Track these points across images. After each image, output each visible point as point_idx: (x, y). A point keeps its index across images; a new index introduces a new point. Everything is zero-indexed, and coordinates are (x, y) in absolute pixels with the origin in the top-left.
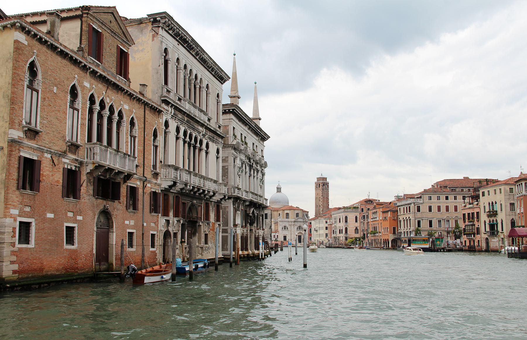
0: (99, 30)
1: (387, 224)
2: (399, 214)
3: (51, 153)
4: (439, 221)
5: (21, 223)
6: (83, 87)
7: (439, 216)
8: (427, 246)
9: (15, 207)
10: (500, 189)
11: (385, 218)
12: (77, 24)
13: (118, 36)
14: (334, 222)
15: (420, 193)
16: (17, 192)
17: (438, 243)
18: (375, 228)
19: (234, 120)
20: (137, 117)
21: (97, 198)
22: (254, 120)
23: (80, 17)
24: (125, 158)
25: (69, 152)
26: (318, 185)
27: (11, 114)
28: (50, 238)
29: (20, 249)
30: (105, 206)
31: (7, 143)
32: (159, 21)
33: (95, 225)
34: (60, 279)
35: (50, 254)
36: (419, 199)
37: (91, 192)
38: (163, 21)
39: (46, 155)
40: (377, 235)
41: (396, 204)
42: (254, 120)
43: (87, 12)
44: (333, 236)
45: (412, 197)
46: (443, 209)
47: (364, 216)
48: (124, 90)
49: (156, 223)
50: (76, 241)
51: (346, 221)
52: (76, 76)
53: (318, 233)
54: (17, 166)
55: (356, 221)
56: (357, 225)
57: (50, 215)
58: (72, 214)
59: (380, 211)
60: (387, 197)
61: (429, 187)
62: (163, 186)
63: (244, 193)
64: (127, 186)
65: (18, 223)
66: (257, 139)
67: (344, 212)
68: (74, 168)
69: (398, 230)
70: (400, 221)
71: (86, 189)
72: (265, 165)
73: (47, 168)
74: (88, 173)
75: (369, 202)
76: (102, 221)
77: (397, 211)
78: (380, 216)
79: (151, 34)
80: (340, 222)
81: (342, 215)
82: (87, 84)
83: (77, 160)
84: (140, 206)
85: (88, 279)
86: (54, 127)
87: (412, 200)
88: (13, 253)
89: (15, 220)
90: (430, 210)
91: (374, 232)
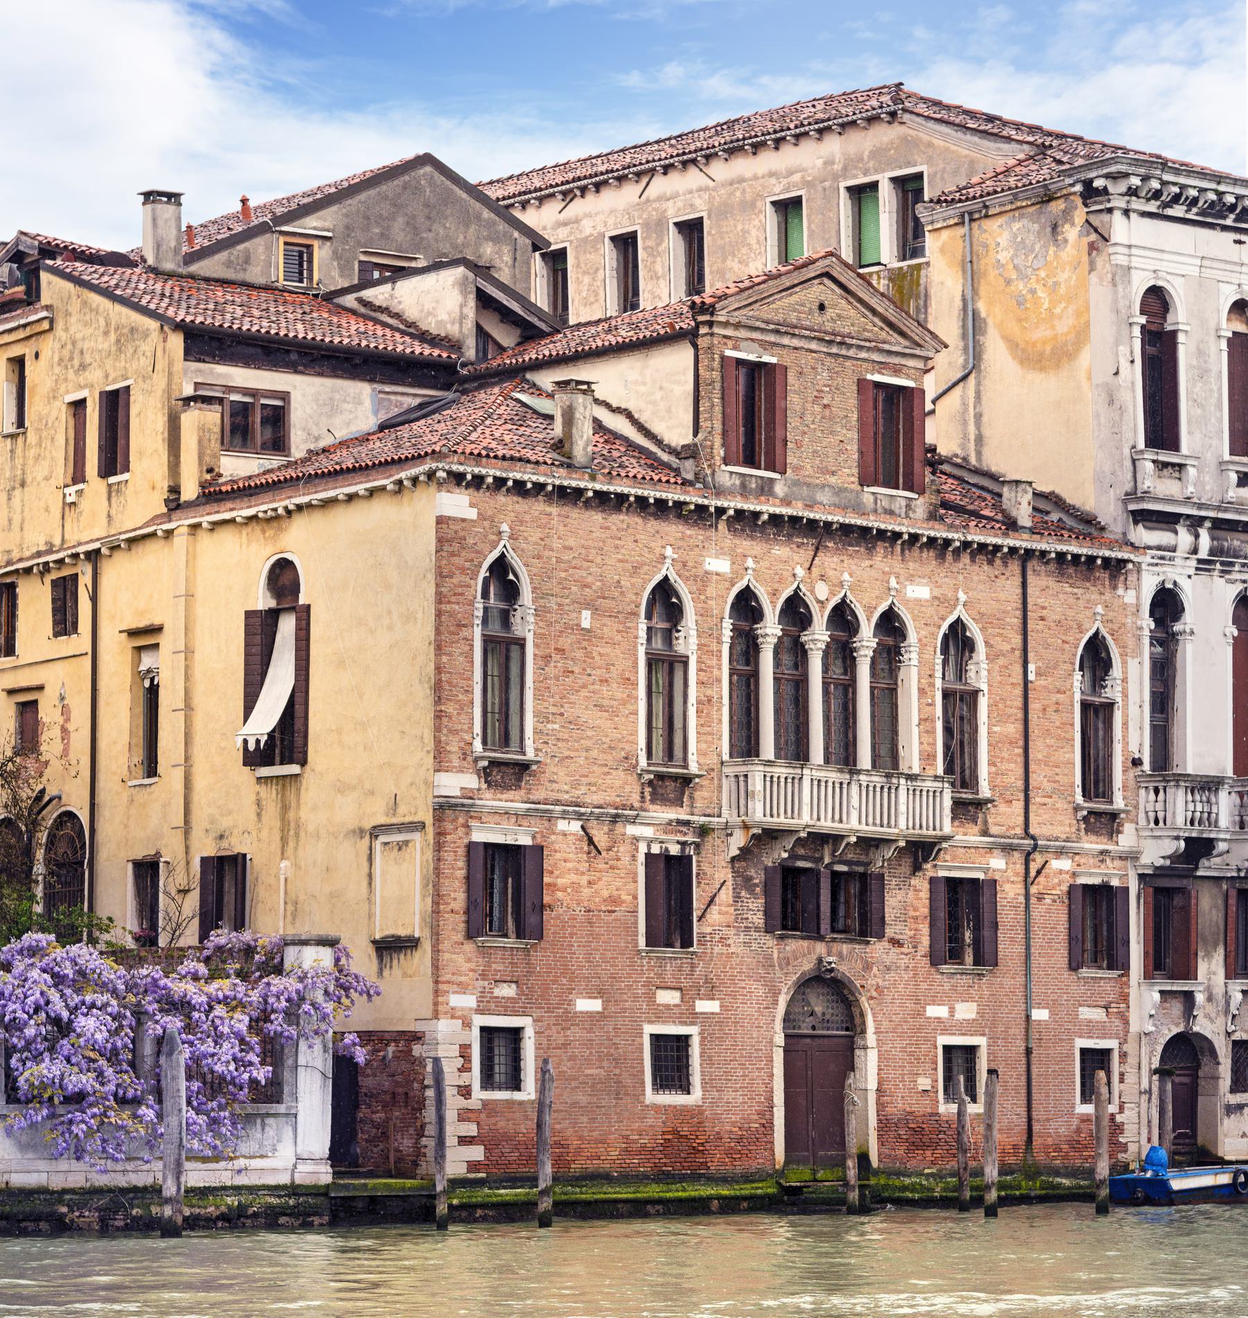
3: (579, 816)
5: (484, 1030)
6: (702, 580)
9: (463, 988)
10: (934, 829)
12: (679, 359)
13: (860, 348)
16: (469, 947)
20: (980, 618)
21: (782, 938)
23: (690, 336)
25: (653, 801)
27: (438, 729)
28: (588, 1072)
29: (485, 1103)
30: (820, 960)
31: (431, 811)
32: (1105, 191)
33: (778, 1025)
35: (593, 1120)
37: (758, 919)
38: (1122, 187)
39: (562, 825)
43: (707, 318)
48: (897, 535)
49: (1118, 1006)
50: (696, 1079)
52: (669, 551)
54: (461, 873)
57: (588, 1005)
58: (677, 994)
62: (1146, 859)
64: (932, 881)
65: (476, 1033)
68: (674, 850)
71: (726, 909)
73: (569, 865)
74: (733, 859)
76: (818, 1009)
79: (1086, 240)
82: (719, 565)
83: (687, 823)
84: (1008, 947)
86: (589, 733)
88: (465, 1115)
89: (467, 1024)
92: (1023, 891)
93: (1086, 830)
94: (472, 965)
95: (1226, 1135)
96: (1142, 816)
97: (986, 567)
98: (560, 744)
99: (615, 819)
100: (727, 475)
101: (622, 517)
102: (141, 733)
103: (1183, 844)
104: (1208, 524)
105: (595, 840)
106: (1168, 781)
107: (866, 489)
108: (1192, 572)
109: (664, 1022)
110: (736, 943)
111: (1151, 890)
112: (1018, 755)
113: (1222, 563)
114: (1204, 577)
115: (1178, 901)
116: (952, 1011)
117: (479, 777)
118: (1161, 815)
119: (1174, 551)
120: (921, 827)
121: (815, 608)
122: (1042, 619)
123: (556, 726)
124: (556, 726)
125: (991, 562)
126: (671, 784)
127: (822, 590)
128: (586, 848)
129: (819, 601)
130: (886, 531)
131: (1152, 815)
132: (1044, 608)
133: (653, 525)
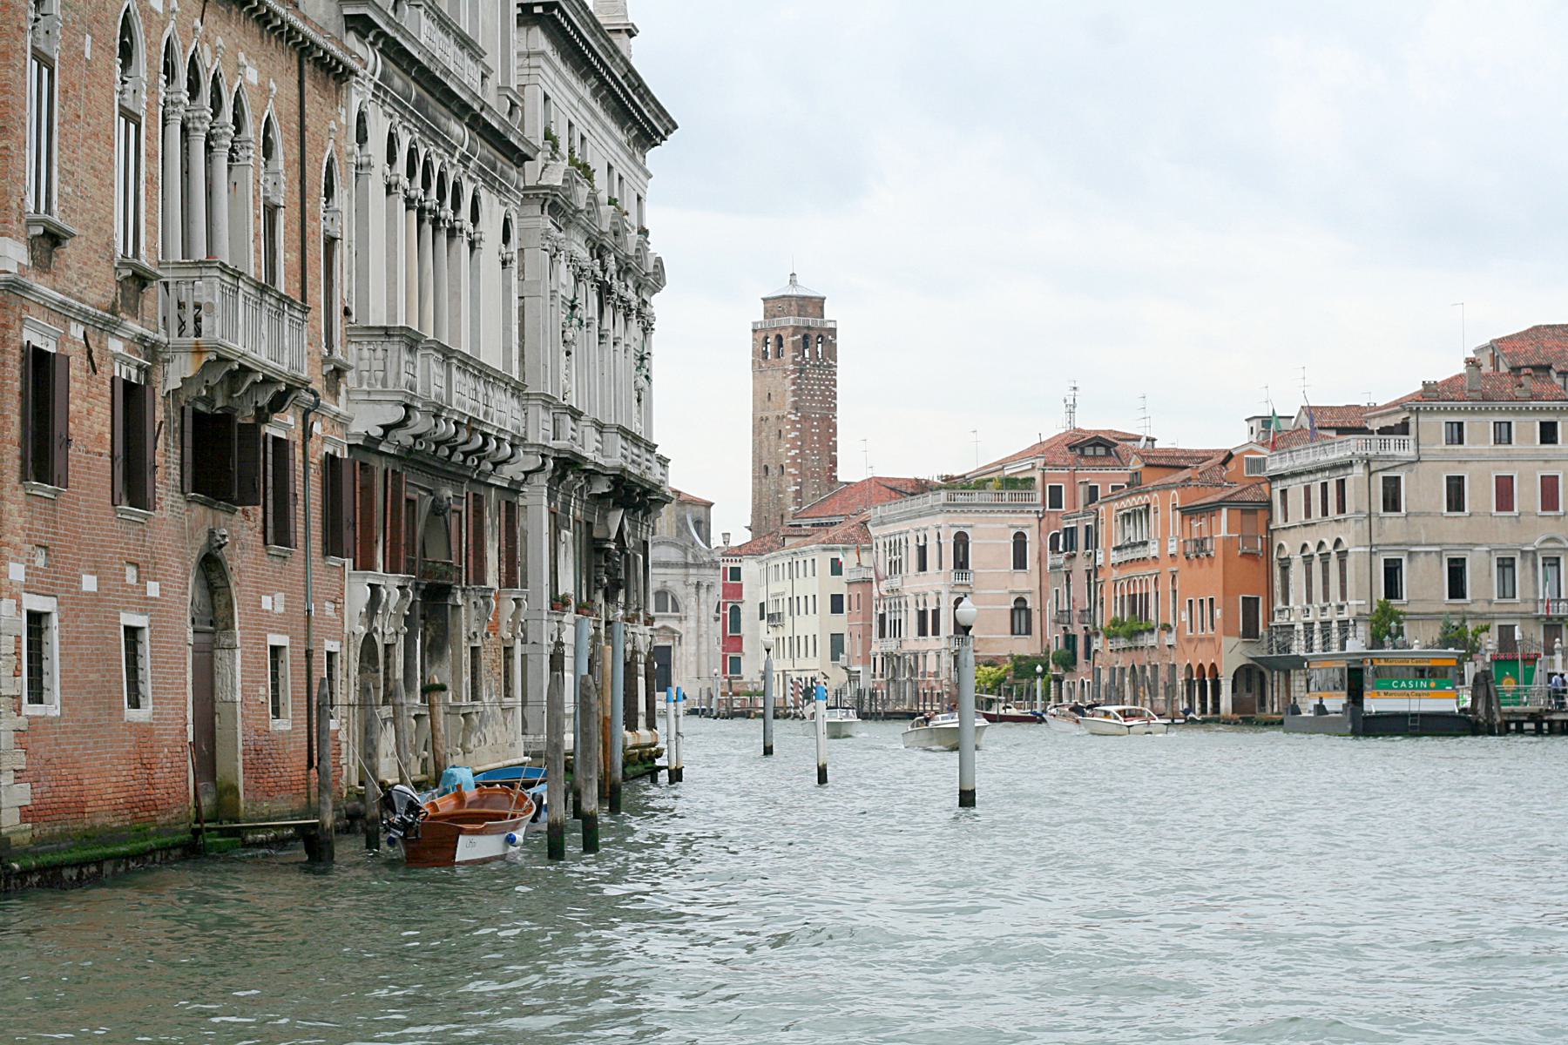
1: (1209, 580)
2: (1278, 521)
4: (1506, 565)
7: (1505, 533)
8: (1447, 705)
11: (1200, 543)
14: (883, 568)
15: (1401, 405)
17: (1508, 685)
18: (1137, 604)
19: (548, 60)
22: (613, 37)
24: (280, 313)
26: (768, 345)
30: (212, 533)
34: (123, 849)
36: (1392, 439)
40: (1149, 640)
41: (1259, 464)
42: (613, 37)
44: (877, 647)
45: (1349, 423)
46: (1527, 495)
47: (1070, 533)
51: (961, 564)
53: (786, 632)
55: (1020, 562)
56: (1026, 582)
59: (1165, 504)
60: (1203, 417)
61: (1447, 366)
63: (592, 435)
66: (623, 138)
67: (950, 506)
69: (1270, 616)
70: (1285, 566)
72: (653, 279)
75: (1097, 447)
77: (1269, 504)
78: (1165, 535)
80: (923, 566)
81: (938, 527)
85: (178, 852)
87: (1351, 447)
90: (1456, 500)
91: (1134, 625)
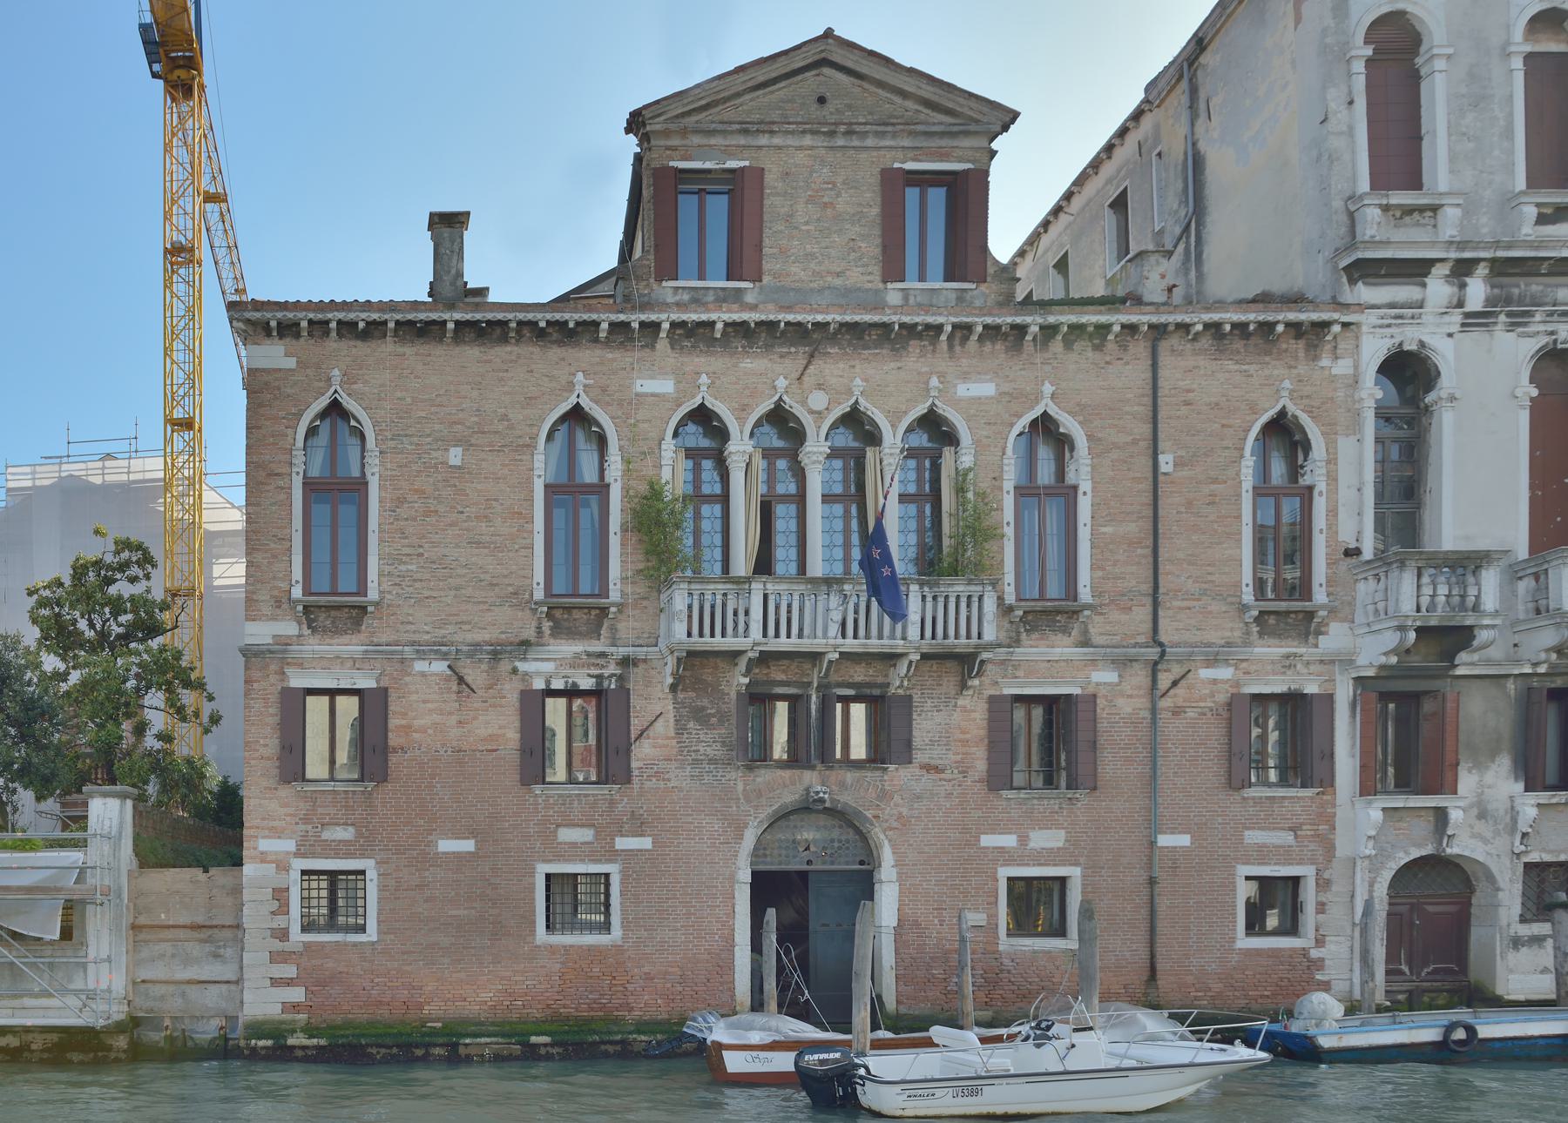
0: (732, 164)
9: (277, 833)
39: (420, 666)
65: (295, 875)
92: (1149, 705)
93: (1261, 634)
94: (291, 810)
95: (1511, 971)
96: (1359, 612)
97: (1090, 354)
98: (417, 585)
99: (496, 656)
100: (670, 292)
101: (509, 349)
102: (1521, 1075)
103: (1412, 635)
104: (1482, 270)
105: (469, 679)
106: (1390, 564)
107: (889, 285)
108: (1455, 328)
109: (567, 861)
110: (679, 777)
111: (1374, 696)
112: (1144, 556)
113: (1509, 315)
114: (1477, 335)
115: (1428, 706)
116: (1023, 840)
117: (300, 624)
118: (1381, 606)
119: (1421, 307)
120: (946, 636)
121: (808, 421)
122: (1187, 403)
123: (413, 567)
124: (413, 567)
125: (1098, 348)
126: (575, 611)
127: (818, 400)
128: (455, 688)
129: (811, 412)
130: (917, 324)
131: (1371, 608)
132: (1189, 391)
133: (555, 352)
